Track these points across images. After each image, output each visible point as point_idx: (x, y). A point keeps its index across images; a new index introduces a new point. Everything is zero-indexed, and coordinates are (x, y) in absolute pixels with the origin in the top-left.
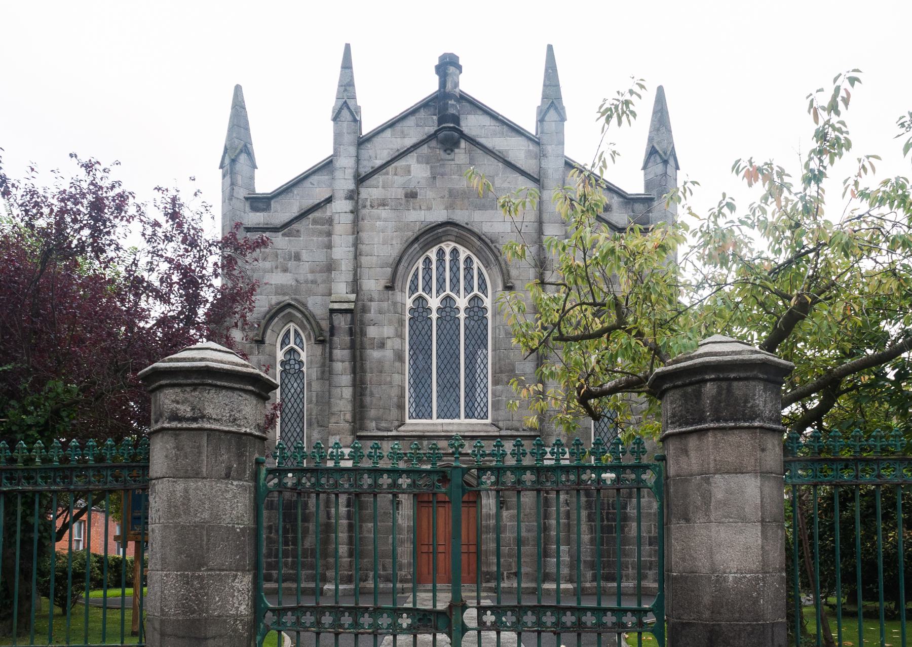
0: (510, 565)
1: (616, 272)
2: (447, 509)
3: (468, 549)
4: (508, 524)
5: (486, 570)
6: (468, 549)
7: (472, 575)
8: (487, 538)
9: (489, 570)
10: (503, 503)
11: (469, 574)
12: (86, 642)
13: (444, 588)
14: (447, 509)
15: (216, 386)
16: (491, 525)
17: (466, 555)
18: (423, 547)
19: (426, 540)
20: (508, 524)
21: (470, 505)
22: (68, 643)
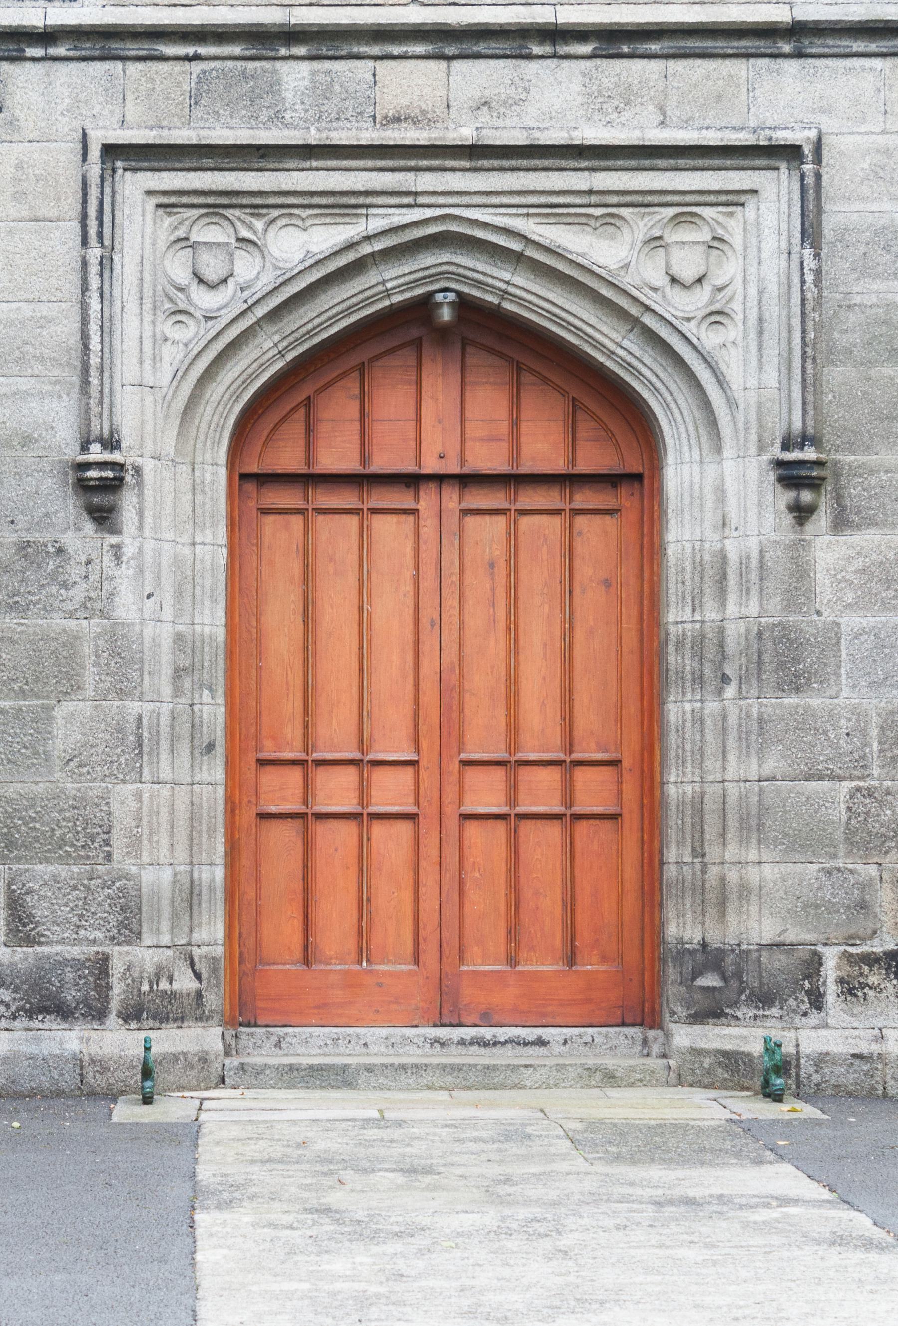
0: (863, 906)
1: (868, 1287)
2: (428, 528)
3: (568, 798)
4: (851, 621)
5: (693, 935)
6: (568, 798)
7: (590, 966)
8: (699, 720)
9: (715, 939)
10: (814, 485)
11: (571, 960)
12: (512, 961)
13: (412, 1055)
14: (428, 528)
15: (642, 677)
16: (734, 632)
17: (553, 832)
18: (271, 778)
19: (293, 732)
20: (851, 621)
21: (584, 498)
22: (512, 961)
